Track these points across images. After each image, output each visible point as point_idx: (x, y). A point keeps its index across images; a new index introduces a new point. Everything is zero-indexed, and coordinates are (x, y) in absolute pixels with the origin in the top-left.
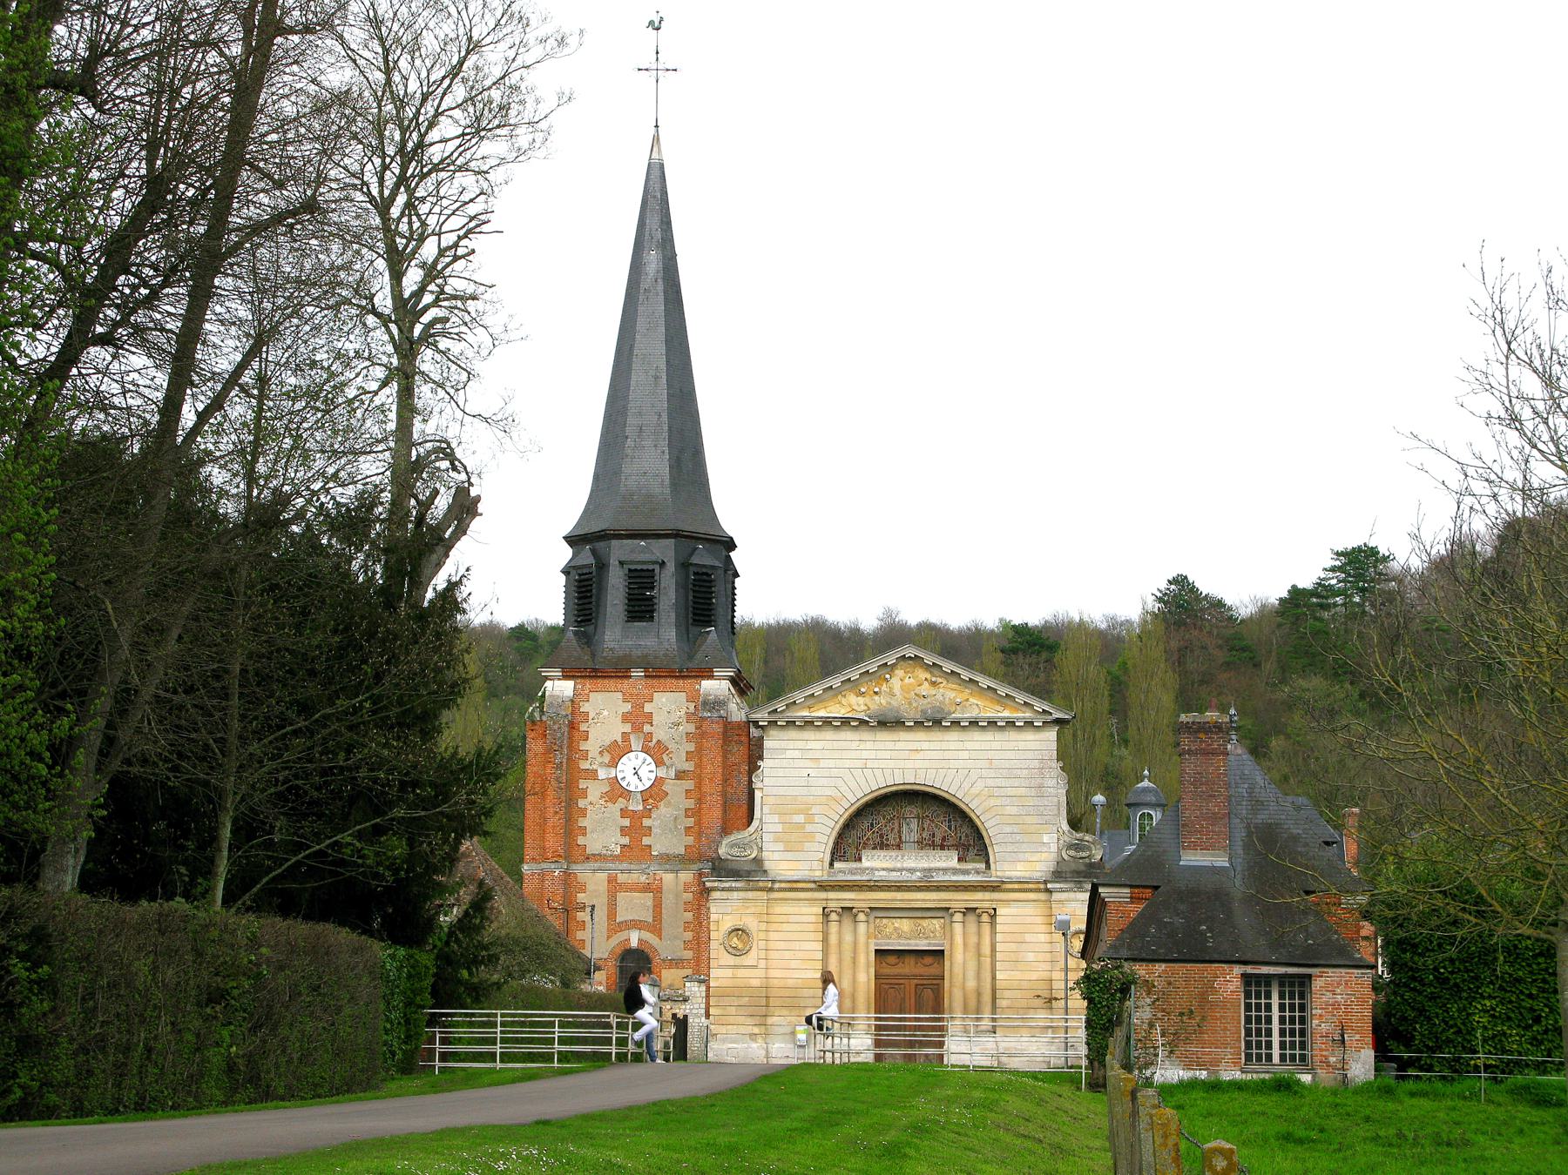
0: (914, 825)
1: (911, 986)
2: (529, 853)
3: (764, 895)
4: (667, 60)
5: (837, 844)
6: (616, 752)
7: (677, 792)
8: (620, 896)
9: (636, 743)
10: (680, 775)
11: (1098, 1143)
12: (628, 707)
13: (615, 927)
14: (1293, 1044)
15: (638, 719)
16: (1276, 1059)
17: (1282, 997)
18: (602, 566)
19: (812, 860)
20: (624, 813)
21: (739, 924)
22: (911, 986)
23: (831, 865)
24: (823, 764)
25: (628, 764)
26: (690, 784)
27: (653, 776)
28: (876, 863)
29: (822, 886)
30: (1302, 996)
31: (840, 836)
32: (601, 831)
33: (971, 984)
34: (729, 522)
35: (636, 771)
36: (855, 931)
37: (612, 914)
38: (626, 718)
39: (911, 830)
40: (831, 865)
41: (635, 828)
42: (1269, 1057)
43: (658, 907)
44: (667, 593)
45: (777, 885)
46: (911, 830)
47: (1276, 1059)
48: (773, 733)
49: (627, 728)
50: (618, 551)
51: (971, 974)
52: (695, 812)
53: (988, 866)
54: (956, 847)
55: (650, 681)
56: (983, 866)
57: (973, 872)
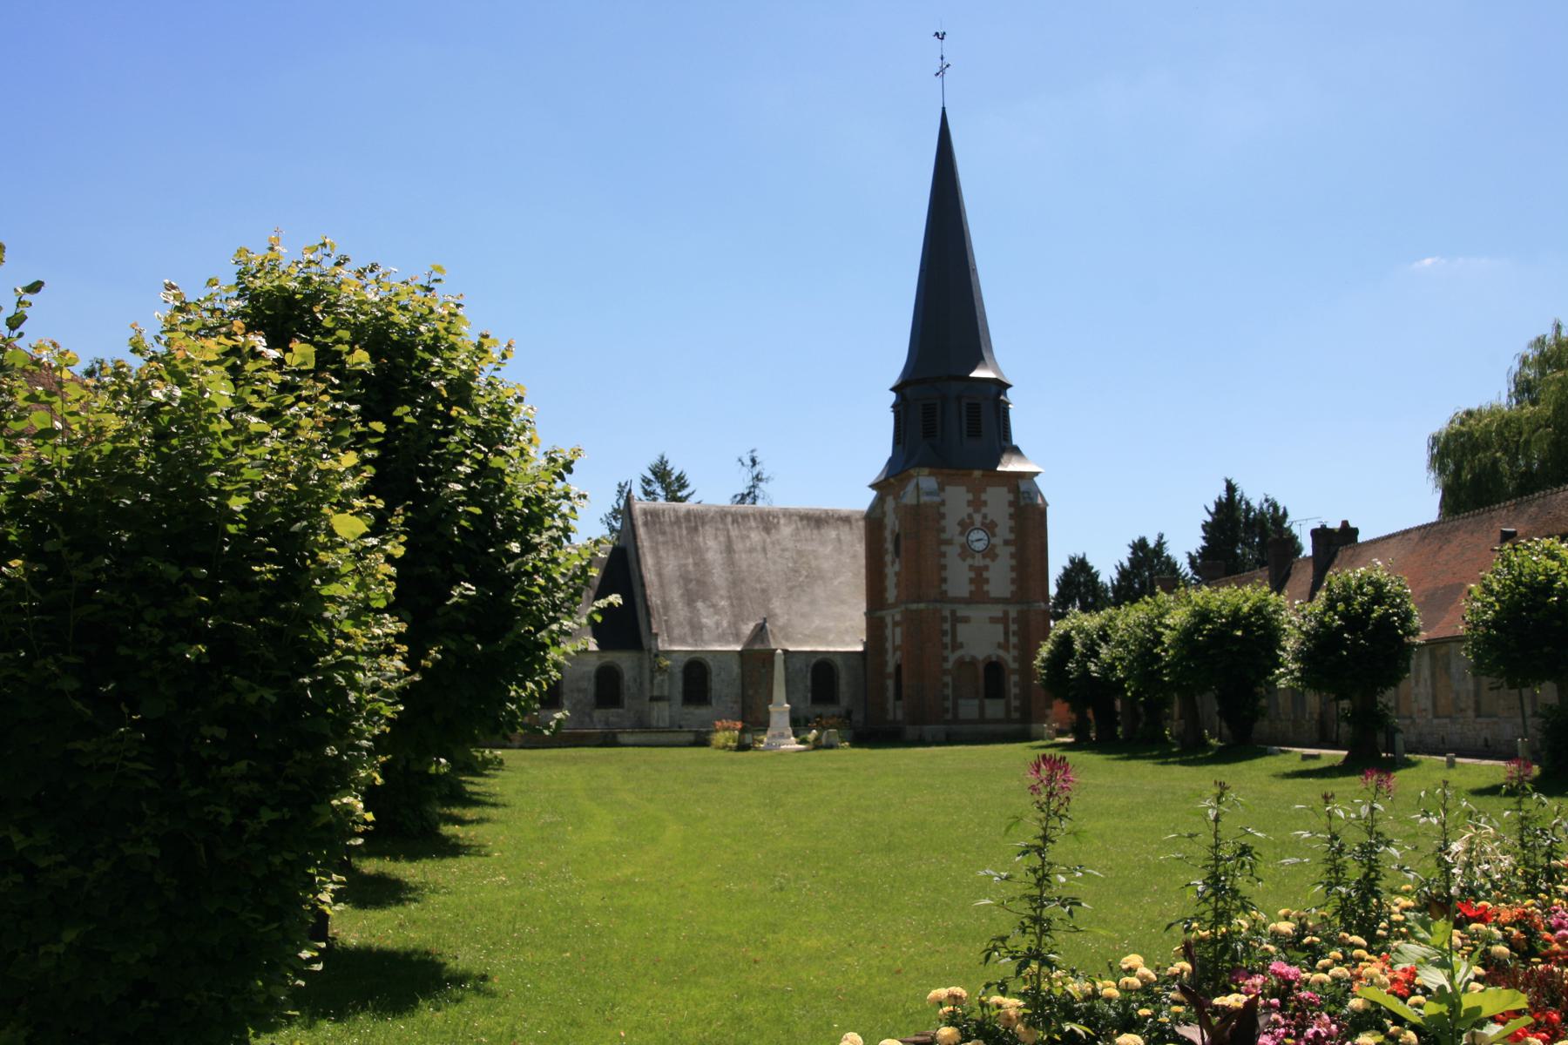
7: (1005, 553)
12: (986, 588)
15: (977, 504)
20: (971, 567)
38: (969, 503)
41: (979, 578)
49: (970, 510)
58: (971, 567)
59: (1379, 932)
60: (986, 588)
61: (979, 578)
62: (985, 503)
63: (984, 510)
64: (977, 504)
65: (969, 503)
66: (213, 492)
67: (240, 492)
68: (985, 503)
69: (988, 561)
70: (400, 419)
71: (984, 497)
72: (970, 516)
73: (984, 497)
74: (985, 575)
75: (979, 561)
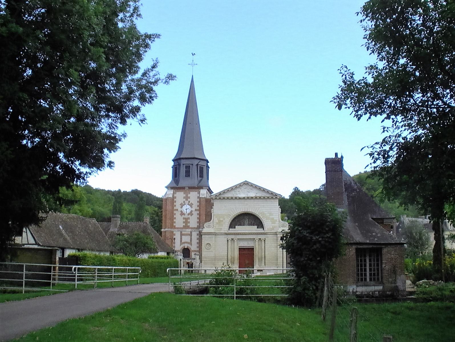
0: (247, 220)
1: (247, 256)
2: (163, 227)
3: (214, 236)
4: (195, 62)
5: (231, 224)
6: (182, 205)
7: (195, 214)
8: (183, 236)
9: (187, 202)
10: (196, 210)
11: (214, 239)
12: (185, 195)
13: (181, 243)
14: (374, 274)
15: (187, 198)
16: (368, 280)
17: (370, 261)
18: (179, 165)
19: (225, 227)
20: (184, 218)
21: (208, 243)
22: (247, 256)
23: (229, 229)
24: (227, 207)
25: (184, 208)
26: (198, 212)
27: (188, 206)
28: (239, 229)
29: (226, 234)
30: (378, 260)
31: (234, 219)
32: (179, 222)
33: (260, 255)
34: (207, 157)
35: (187, 209)
36: (234, 244)
37: (181, 241)
38: (184, 198)
39: (247, 221)
40: (229, 229)
41: (186, 221)
42: (366, 279)
43: (191, 240)
44: (194, 171)
45: (217, 234)
46: (247, 221)
47: (368, 280)
48: (216, 201)
49: (185, 200)
50: (183, 162)
51: (186, 233)
52: (199, 218)
53: (263, 229)
54: (257, 225)
55: (190, 190)
56: (262, 229)
57: (260, 230)
58: (184, 218)
59: (289, 235)
60: (185, 195)
61: (186, 221)
62: (189, 198)
63: (189, 200)
64: (187, 198)
65: (184, 198)
66: (37, 19)
67: (393, 68)
68: (189, 198)
69: (190, 216)
70: (23, 59)
71: (189, 195)
72: (184, 202)
73: (189, 195)
74: (188, 220)
75: (186, 216)
